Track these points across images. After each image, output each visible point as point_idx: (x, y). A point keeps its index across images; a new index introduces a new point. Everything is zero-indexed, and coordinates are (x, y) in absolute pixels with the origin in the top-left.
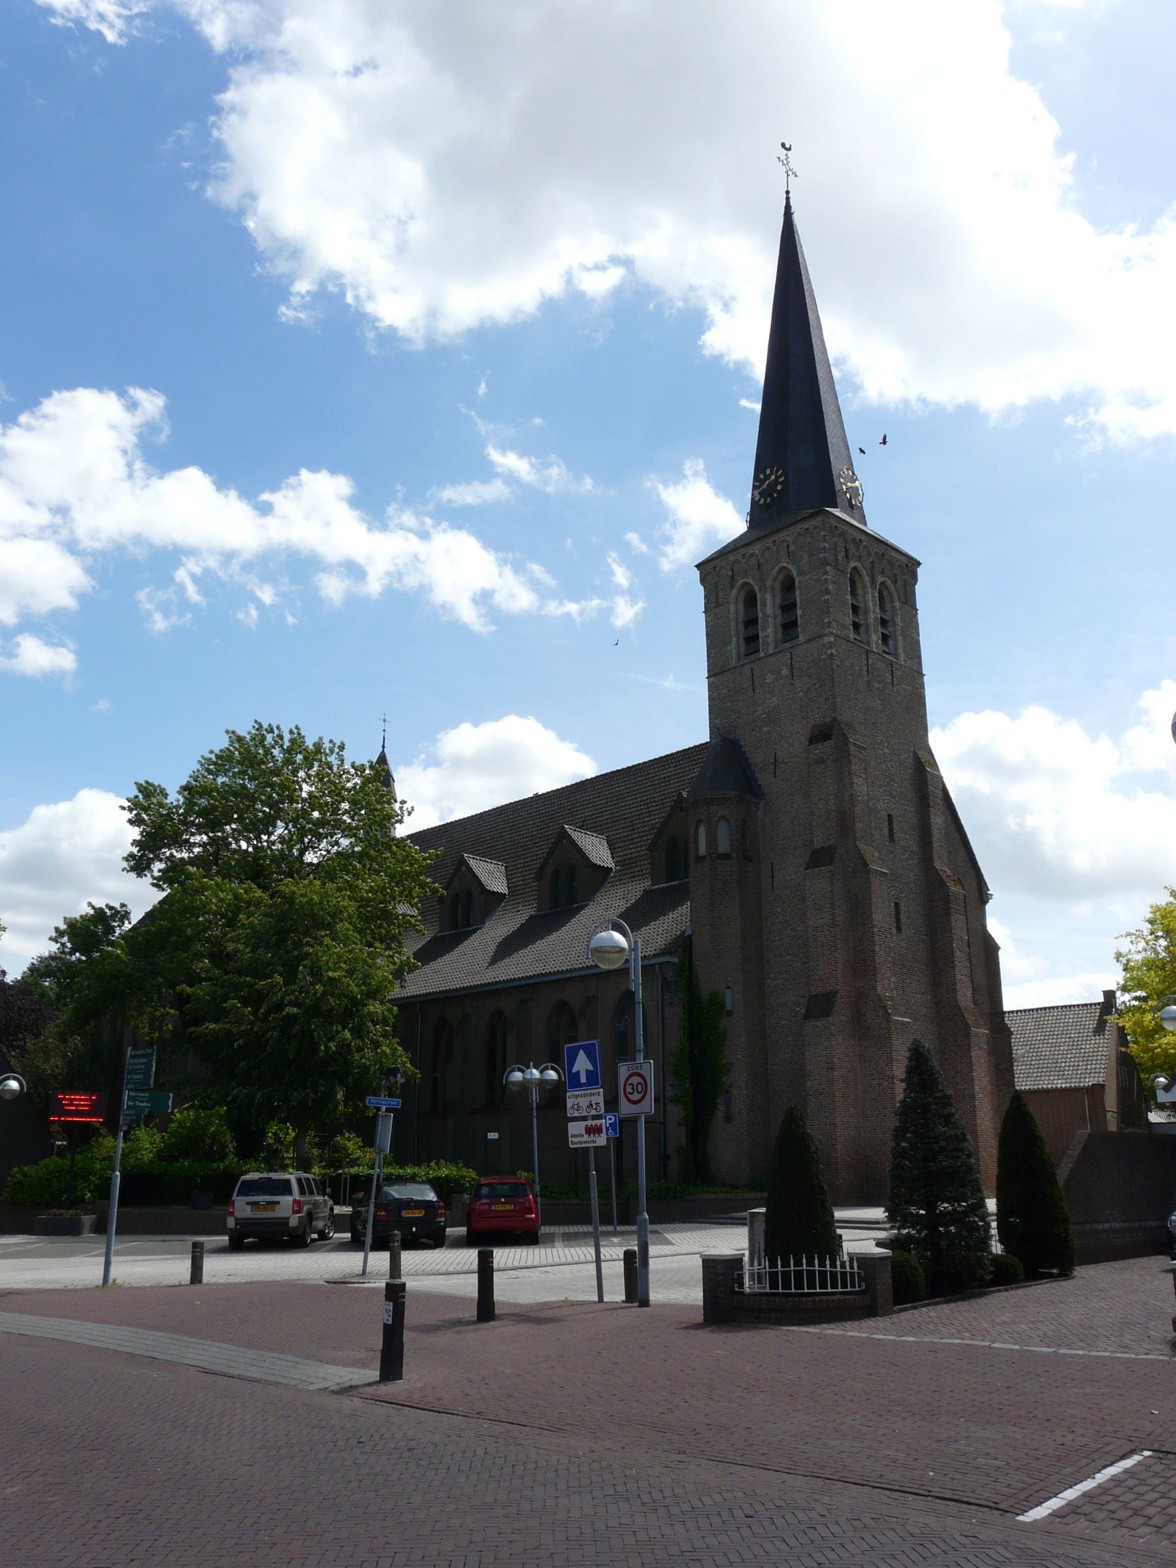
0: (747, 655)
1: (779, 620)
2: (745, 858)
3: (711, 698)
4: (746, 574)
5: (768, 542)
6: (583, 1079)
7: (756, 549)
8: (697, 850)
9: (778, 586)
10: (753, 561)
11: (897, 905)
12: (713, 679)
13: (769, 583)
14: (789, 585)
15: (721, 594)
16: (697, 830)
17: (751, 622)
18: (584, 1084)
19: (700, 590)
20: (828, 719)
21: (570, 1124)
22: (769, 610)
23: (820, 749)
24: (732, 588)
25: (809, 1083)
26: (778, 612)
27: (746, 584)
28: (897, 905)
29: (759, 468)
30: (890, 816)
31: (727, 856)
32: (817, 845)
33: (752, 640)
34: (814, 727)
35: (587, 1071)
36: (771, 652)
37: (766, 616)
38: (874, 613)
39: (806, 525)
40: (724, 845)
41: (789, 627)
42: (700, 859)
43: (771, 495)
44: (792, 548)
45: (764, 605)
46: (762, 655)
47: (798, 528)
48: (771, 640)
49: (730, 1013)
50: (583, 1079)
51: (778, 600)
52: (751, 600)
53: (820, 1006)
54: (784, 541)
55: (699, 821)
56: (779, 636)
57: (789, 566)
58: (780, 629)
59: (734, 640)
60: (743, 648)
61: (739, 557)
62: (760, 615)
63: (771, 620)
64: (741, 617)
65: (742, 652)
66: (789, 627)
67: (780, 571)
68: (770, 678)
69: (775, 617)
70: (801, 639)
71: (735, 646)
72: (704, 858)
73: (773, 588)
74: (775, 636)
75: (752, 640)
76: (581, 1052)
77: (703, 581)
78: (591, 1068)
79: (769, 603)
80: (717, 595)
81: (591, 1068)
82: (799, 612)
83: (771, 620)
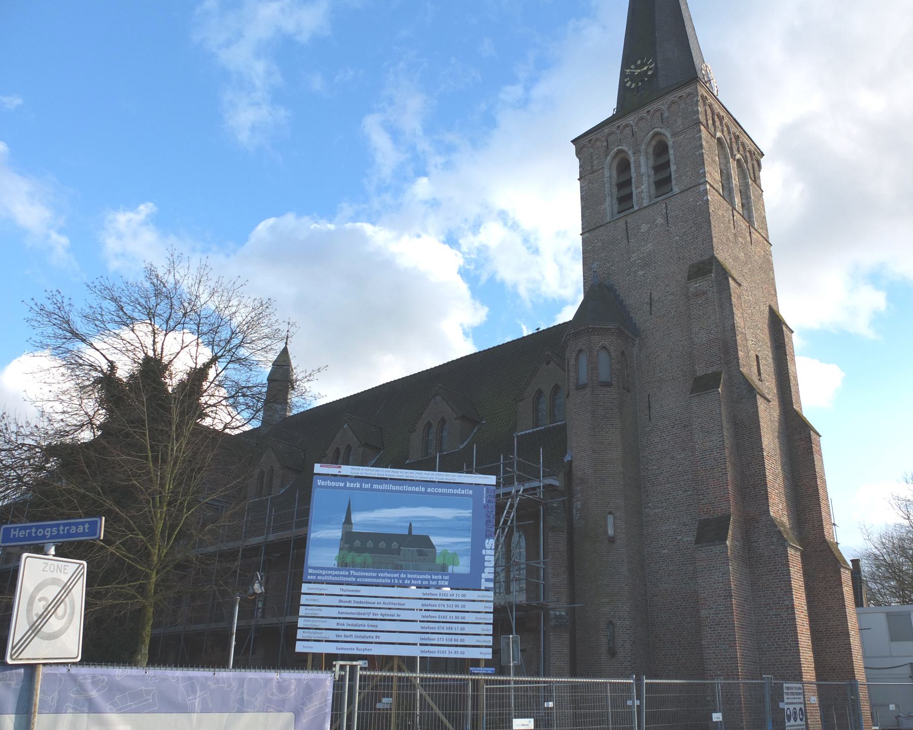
0: (619, 212)
1: (652, 180)
4: (620, 142)
9: (651, 150)
10: (628, 131)
12: (587, 235)
13: (643, 147)
14: (661, 149)
15: (595, 162)
16: (577, 359)
17: (624, 184)
19: (576, 162)
20: (706, 257)
21: (297, 643)
22: (643, 169)
23: (695, 286)
24: (607, 156)
25: (703, 613)
26: (652, 172)
27: (620, 151)
29: (626, 63)
30: (757, 357)
31: (608, 384)
32: (700, 373)
33: (625, 200)
34: (691, 266)
36: (645, 205)
37: (640, 175)
38: (735, 181)
41: (663, 183)
42: (580, 387)
45: (638, 166)
46: (636, 208)
47: (671, 98)
48: (645, 195)
49: (612, 540)
50: (532, 563)
51: (651, 163)
52: (624, 166)
53: (711, 531)
54: (657, 111)
55: (580, 351)
56: (653, 192)
57: (663, 131)
58: (653, 187)
59: (608, 199)
61: (614, 129)
62: (634, 175)
64: (614, 180)
65: (616, 210)
66: (663, 183)
68: (644, 228)
69: (649, 176)
70: (676, 190)
71: (609, 205)
72: (584, 387)
73: (647, 153)
74: (649, 192)
75: (625, 200)
77: (578, 153)
80: (592, 163)
82: (673, 168)
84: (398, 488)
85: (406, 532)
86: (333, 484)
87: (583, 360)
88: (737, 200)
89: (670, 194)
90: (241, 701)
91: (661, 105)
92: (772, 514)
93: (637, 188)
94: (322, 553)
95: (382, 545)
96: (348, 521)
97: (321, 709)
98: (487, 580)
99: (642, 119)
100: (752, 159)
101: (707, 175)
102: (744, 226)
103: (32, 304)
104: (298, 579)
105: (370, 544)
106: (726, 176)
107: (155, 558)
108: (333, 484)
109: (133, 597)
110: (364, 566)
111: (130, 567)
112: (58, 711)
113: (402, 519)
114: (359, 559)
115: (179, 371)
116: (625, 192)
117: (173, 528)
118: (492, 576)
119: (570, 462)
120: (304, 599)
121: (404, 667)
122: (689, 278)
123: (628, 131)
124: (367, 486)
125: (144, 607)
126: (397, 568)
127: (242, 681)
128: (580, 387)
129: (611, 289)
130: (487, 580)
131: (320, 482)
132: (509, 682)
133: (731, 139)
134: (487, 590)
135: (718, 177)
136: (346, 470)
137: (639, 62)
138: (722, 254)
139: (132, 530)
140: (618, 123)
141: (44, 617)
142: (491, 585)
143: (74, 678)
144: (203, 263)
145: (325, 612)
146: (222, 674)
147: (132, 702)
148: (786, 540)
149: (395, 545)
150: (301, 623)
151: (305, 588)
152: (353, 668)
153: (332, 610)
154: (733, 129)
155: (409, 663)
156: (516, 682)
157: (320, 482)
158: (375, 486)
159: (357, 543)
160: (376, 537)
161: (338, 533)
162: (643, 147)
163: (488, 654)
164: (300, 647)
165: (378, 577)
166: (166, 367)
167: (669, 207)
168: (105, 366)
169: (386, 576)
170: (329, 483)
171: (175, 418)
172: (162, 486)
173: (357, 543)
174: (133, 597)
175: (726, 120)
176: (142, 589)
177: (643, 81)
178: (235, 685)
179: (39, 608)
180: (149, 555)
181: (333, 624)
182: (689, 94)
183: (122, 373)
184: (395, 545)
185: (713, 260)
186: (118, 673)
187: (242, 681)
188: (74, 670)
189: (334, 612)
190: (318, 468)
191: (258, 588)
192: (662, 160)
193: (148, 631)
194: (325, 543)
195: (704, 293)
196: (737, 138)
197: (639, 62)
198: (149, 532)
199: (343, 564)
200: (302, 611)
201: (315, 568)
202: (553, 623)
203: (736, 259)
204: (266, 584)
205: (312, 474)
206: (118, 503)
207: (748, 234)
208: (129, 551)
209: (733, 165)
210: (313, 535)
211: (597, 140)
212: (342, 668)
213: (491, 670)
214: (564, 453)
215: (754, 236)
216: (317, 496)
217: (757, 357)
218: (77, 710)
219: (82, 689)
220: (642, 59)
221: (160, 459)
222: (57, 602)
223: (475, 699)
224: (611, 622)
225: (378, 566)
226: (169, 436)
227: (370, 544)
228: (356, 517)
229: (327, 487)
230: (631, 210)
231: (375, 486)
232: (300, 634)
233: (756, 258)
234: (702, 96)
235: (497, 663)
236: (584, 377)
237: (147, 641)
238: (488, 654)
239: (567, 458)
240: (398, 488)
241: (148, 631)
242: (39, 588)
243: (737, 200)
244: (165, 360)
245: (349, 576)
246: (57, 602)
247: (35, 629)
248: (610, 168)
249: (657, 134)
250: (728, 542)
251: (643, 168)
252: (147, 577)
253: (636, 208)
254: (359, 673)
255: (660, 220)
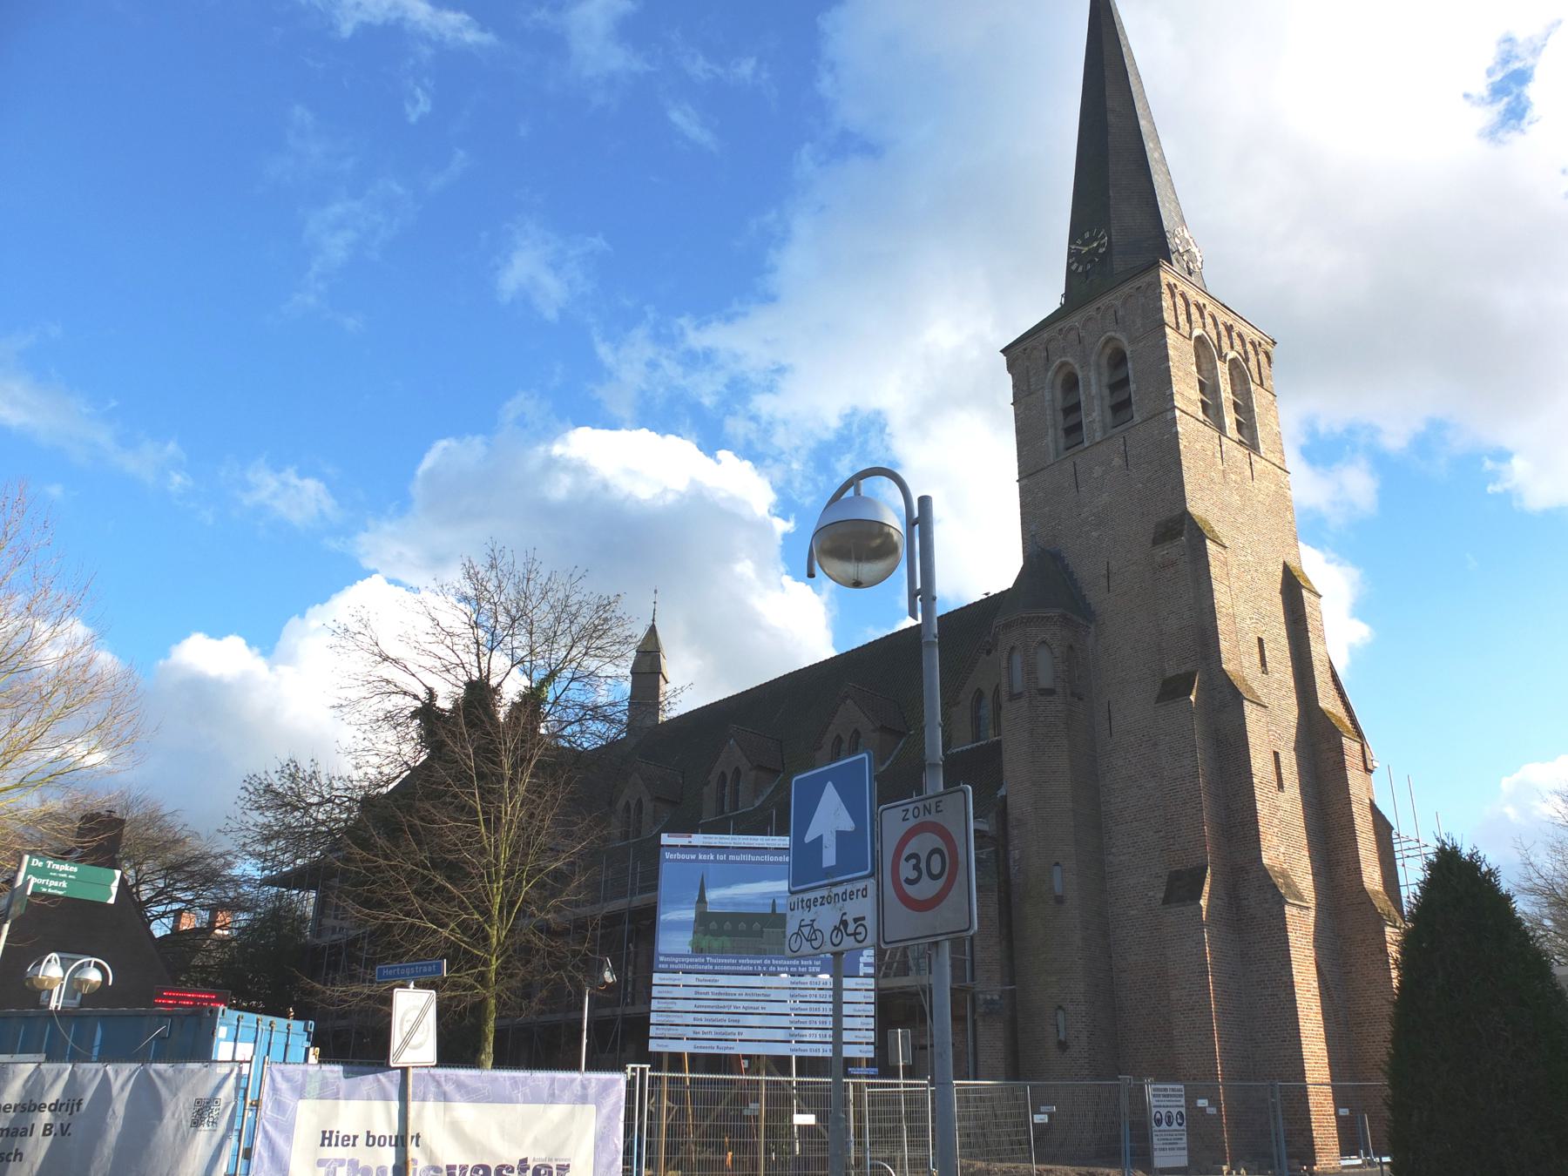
1: (1107, 402)
2: (1073, 694)
3: (1022, 514)
5: (1090, 310)
6: (829, 858)
7: (1076, 320)
8: (1011, 686)
9: (1104, 361)
10: (1072, 336)
11: (1276, 754)
12: (1025, 481)
13: (1093, 358)
14: (1119, 359)
16: (1009, 659)
17: (1072, 409)
18: (829, 872)
20: (1177, 512)
23: (1162, 552)
24: (1047, 370)
26: (1106, 392)
28: (1276, 754)
30: (1260, 640)
31: (1050, 692)
32: (1170, 673)
35: (841, 835)
38: (1226, 393)
39: (1137, 283)
40: (1045, 679)
41: (1121, 408)
43: (1092, 261)
44: (1120, 313)
45: (1088, 385)
47: (1126, 289)
48: (1097, 426)
49: (1060, 900)
50: (829, 858)
52: (1071, 383)
55: (1013, 648)
57: (1118, 335)
58: (1108, 413)
60: (1062, 443)
62: (1083, 398)
63: (1096, 402)
64: (1059, 404)
65: (1062, 445)
66: (1121, 408)
67: (1107, 343)
68: (1098, 471)
69: (1102, 398)
70: (1137, 418)
71: (1051, 439)
73: (1098, 365)
76: (830, 789)
77: (1011, 367)
78: (847, 824)
79: (1093, 381)
81: (847, 824)
82: (1133, 387)
83: (1096, 402)
84: (758, 858)
85: (769, 911)
86: (683, 857)
87: (1017, 659)
88: (1230, 418)
89: (1129, 424)
90: (553, 1095)
91: (1113, 299)
92: (1265, 861)
93: (1087, 415)
94: (673, 940)
95: (742, 926)
96: (702, 899)
97: (617, 1103)
98: (866, 965)
99: (1090, 319)
100: (1257, 354)
101: (1177, 397)
102: (1240, 456)
103: (334, 626)
104: (650, 969)
105: (728, 926)
106: (1208, 388)
107: (494, 940)
108: (683, 857)
109: (472, 987)
110: (722, 952)
111: (466, 952)
112: (424, 1100)
113: (763, 895)
114: (716, 944)
115: (512, 687)
116: (1072, 420)
117: (512, 904)
118: (872, 960)
119: (1004, 798)
120: (655, 992)
121: (773, 1068)
122: (1155, 542)
123: (1072, 336)
124: (722, 857)
125: (485, 999)
126: (760, 953)
127: (553, 1081)
128: (1013, 697)
129: (1056, 557)
130: (866, 965)
131: (668, 855)
132: (897, 1085)
133: (1219, 334)
134: (866, 976)
135: (1196, 395)
136: (698, 839)
137: (1087, 235)
138: (1199, 504)
139: (465, 909)
140: (1059, 326)
141: (411, 1033)
142: (871, 970)
143: (433, 1077)
144: (530, 555)
145: (680, 1005)
146: (485, 1073)
147: (472, 1095)
148: (1282, 897)
149: (757, 926)
150: (654, 1018)
151: (656, 978)
152: (642, 1070)
153: (689, 1006)
154: (1222, 318)
155: (781, 1064)
156: (905, 1085)
157: (668, 855)
158: (732, 857)
159: (713, 925)
160: (735, 917)
161: (690, 914)
162: (1093, 358)
163: (869, 1052)
164: (654, 1046)
165: (738, 964)
166: (495, 691)
167: (1129, 442)
168: (423, 695)
169: (747, 962)
170: (678, 856)
171: (507, 763)
172: (497, 858)
173: (713, 925)
174: (472, 987)
175: (1210, 308)
176: (482, 978)
177: (1092, 261)
178: (547, 1083)
179: (407, 1028)
180: (486, 938)
181: (689, 1019)
182: (1149, 284)
183: (444, 703)
184: (757, 926)
185: (1186, 516)
186: (463, 1074)
187: (553, 1081)
188: (433, 1071)
189: (690, 1006)
190: (666, 839)
191: (608, 977)
192: (1120, 375)
193: (490, 1027)
194: (678, 926)
195: (1173, 564)
196: (1229, 329)
197: (1087, 235)
198: (486, 913)
199: (698, 950)
200: (655, 1005)
201: (666, 955)
202: (981, 1010)
203: (1224, 507)
204: (614, 971)
205: (658, 846)
206: (449, 878)
207: (1247, 467)
208: (463, 933)
209: (1223, 370)
210: (662, 917)
211: (1035, 348)
212: (634, 1070)
213: (873, 1071)
214: (999, 785)
215: (1256, 467)
216: (665, 869)
217: (1260, 640)
218: (436, 1100)
219: (439, 1084)
220: (1091, 231)
221: (493, 823)
222: (418, 1022)
223: (858, 1101)
224: (1060, 1007)
225: (738, 952)
226: (501, 795)
227: (728, 926)
228: (712, 895)
229: (676, 860)
230: (1080, 447)
231: (732, 857)
232: (653, 1031)
233: (1261, 497)
234: (1169, 285)
235: (882, 1064)
236: (1018, 687)
237: (491, 1038)
238: (869, 1052)
239: (1002, 792)
240: (758, 858)
241: (490, 1027)
242: (405, 1014)
243: (1230, 418)
244: (493, 682)
245: (705, 963)
246: (418, 1022)
247: (405, 1042)
248: (1053, 387)
249: (1110, 339)
250: (1203, 902)
251: (1094, 388)
252: (486, 963)
253: (1086, 444)
254: (648, 1074)
255: (1117, 461)
